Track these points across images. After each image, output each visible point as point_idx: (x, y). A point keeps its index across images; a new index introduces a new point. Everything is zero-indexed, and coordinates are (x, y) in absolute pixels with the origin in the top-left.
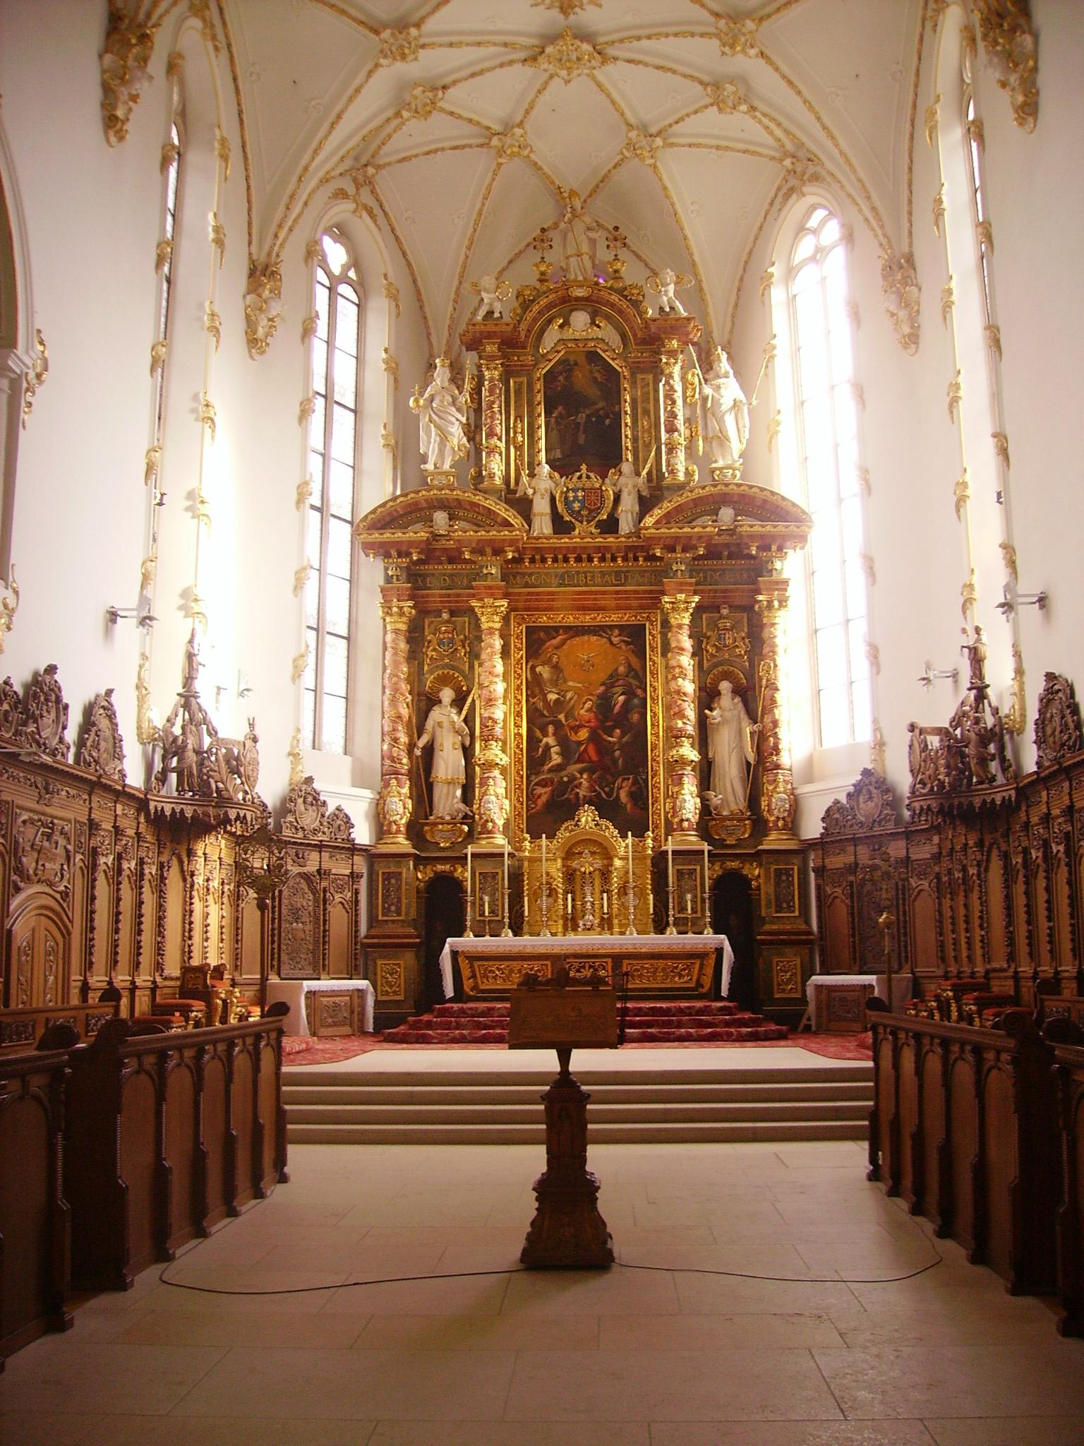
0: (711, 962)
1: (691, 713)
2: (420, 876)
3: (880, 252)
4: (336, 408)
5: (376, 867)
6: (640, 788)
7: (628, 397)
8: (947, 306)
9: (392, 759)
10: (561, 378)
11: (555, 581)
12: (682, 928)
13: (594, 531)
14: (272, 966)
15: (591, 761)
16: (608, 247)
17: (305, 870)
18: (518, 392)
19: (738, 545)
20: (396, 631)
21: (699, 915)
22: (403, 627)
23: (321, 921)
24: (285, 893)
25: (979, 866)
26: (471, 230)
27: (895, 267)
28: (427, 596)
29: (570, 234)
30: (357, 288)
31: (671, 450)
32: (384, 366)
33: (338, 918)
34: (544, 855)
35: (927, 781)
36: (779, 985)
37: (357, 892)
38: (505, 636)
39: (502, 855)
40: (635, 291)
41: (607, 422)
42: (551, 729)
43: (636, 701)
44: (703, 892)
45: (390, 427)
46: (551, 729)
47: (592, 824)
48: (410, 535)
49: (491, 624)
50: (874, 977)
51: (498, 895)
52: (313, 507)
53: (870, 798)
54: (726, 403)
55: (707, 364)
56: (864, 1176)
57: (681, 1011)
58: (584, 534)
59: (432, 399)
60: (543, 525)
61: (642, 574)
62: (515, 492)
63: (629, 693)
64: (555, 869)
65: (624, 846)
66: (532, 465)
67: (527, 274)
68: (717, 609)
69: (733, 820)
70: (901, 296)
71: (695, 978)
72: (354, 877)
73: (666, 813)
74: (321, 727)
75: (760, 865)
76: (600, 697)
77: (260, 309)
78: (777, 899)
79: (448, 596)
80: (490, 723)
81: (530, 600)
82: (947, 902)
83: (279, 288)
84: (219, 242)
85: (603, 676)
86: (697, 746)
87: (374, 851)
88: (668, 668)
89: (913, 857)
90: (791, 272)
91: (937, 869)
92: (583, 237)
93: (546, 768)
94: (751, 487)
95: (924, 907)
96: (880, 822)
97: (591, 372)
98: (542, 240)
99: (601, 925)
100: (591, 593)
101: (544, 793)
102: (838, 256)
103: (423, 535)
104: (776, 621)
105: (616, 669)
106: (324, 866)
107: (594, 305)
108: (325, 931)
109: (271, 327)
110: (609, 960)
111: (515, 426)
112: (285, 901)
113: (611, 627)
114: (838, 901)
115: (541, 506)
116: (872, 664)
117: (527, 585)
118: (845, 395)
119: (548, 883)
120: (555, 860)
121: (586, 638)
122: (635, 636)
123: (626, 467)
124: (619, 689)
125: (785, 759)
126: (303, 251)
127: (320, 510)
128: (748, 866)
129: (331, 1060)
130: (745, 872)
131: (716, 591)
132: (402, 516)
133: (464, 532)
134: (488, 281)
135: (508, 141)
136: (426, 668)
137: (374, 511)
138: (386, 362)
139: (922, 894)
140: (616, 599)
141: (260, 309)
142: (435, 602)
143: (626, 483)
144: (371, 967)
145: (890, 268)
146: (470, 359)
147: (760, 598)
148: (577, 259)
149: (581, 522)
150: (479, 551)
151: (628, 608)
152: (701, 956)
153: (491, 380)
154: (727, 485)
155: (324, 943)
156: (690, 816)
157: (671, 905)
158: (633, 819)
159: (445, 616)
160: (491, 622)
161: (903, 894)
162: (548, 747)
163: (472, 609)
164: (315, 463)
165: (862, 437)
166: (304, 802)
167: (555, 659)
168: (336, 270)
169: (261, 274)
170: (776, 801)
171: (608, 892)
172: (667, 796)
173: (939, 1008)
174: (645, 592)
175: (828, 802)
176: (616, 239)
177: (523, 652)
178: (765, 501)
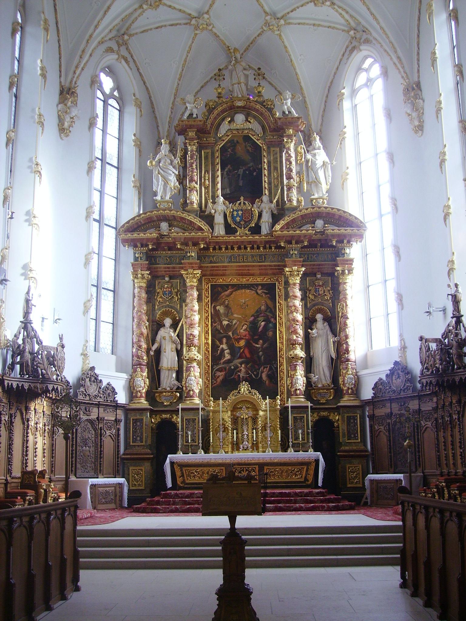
0: (313, 467)
1: (301, 332)
2: (153, 421)
3: (402, 81)
5: (129, 416)
7: (266, 161)
8: (439, 110)
9: (138, 357)
10: (229, 150)
12: (297, 449)
13: (247, 232)
15: (246, 357)
16: (255, 79)
17: (90, 418)
18: (206, 158)
19: (326, 240)
20: (140, 287)
22: (144, 285)
23: (99, 446)
26: (180, 70)
28: (157, 268)
29: (234, 73)
31: (290, 188)
32: (133, 144)
33: (108, 444)
34: (221, 409)
35: (430, 367)
36: (350, 480)
37: (119, 430)
39: (198, 409)
40: (269, 103)
41: (255, 174)
42: (224, 340)
44: (308, 428)
45: (137, 176)
46: (224, 340)
47: (247, 392)
50: (402, 475)
53: (399, 377)
54: (319, 163)
55: (308, 142)
57: (296, 494)
58: (242, 234)
60: (220, 230)
62: (205, 212)
63: (267, 320)
64: (227, 417)
65: (265, 404)
66: (214, 197)
67: (211, 94)
68: (315, 275)
72: (117, 421)
73: (288, 386)
78: (349, 432)
79: (168, 268)
81: (213, 270)
82: (441, 434)
84: (44, 76)
85: (253, 312)
87: (128, 407)
90: (354, 92)
91: (436, 416)
92: (241, 73)
93: (222, 361)
94: (333, 209)
95: (429, 436)
96: (404, 390)
97: (246, 147)
99: (252, 447)
100: (246, 266)
101: (221, 375)
102: (379, 85)
103: (155, 235)
104: (347, 281)
105: (260, 308)
107: (247, 111)
111: (204, 176)
113: (257, 285)
114: (381, 433)
115: (219, 219)
116: (399, 304)
119: (223, 424)
122: (270, 289)
123: (265, 198)
124: (261, 319)
127: (99, 221)
128: (332, 414)
129: (104, 523)
130: (331, 418)
133: (177, 233)
134: (190, 98)
135: (201, 21)
136: (156, 307)
137: (128, 222)
139: (428, 429)
141: (66, 112)
142: (161, 271)
143: (265, 206)
146: (180, 140)
147: (338, 268)
148: (238, 85)
149: (241, 228)
151: (267, 274)
153: (192, 151)
154: (319, 208)
155: (101, 458)
156: (300, 387)
159: (167, 279)
160: (192, 282)
161: (418, 429)
162: (223, 350)
163: (181, 275)
164: (96, 196)
165: (392, 181)
166: (90, 380)
168: (108, 91)
169: (66, 93)
170: (347, 379)
172: (288, 376)
174: (275, 266)
176: (259, 75)
178: (340, 216)
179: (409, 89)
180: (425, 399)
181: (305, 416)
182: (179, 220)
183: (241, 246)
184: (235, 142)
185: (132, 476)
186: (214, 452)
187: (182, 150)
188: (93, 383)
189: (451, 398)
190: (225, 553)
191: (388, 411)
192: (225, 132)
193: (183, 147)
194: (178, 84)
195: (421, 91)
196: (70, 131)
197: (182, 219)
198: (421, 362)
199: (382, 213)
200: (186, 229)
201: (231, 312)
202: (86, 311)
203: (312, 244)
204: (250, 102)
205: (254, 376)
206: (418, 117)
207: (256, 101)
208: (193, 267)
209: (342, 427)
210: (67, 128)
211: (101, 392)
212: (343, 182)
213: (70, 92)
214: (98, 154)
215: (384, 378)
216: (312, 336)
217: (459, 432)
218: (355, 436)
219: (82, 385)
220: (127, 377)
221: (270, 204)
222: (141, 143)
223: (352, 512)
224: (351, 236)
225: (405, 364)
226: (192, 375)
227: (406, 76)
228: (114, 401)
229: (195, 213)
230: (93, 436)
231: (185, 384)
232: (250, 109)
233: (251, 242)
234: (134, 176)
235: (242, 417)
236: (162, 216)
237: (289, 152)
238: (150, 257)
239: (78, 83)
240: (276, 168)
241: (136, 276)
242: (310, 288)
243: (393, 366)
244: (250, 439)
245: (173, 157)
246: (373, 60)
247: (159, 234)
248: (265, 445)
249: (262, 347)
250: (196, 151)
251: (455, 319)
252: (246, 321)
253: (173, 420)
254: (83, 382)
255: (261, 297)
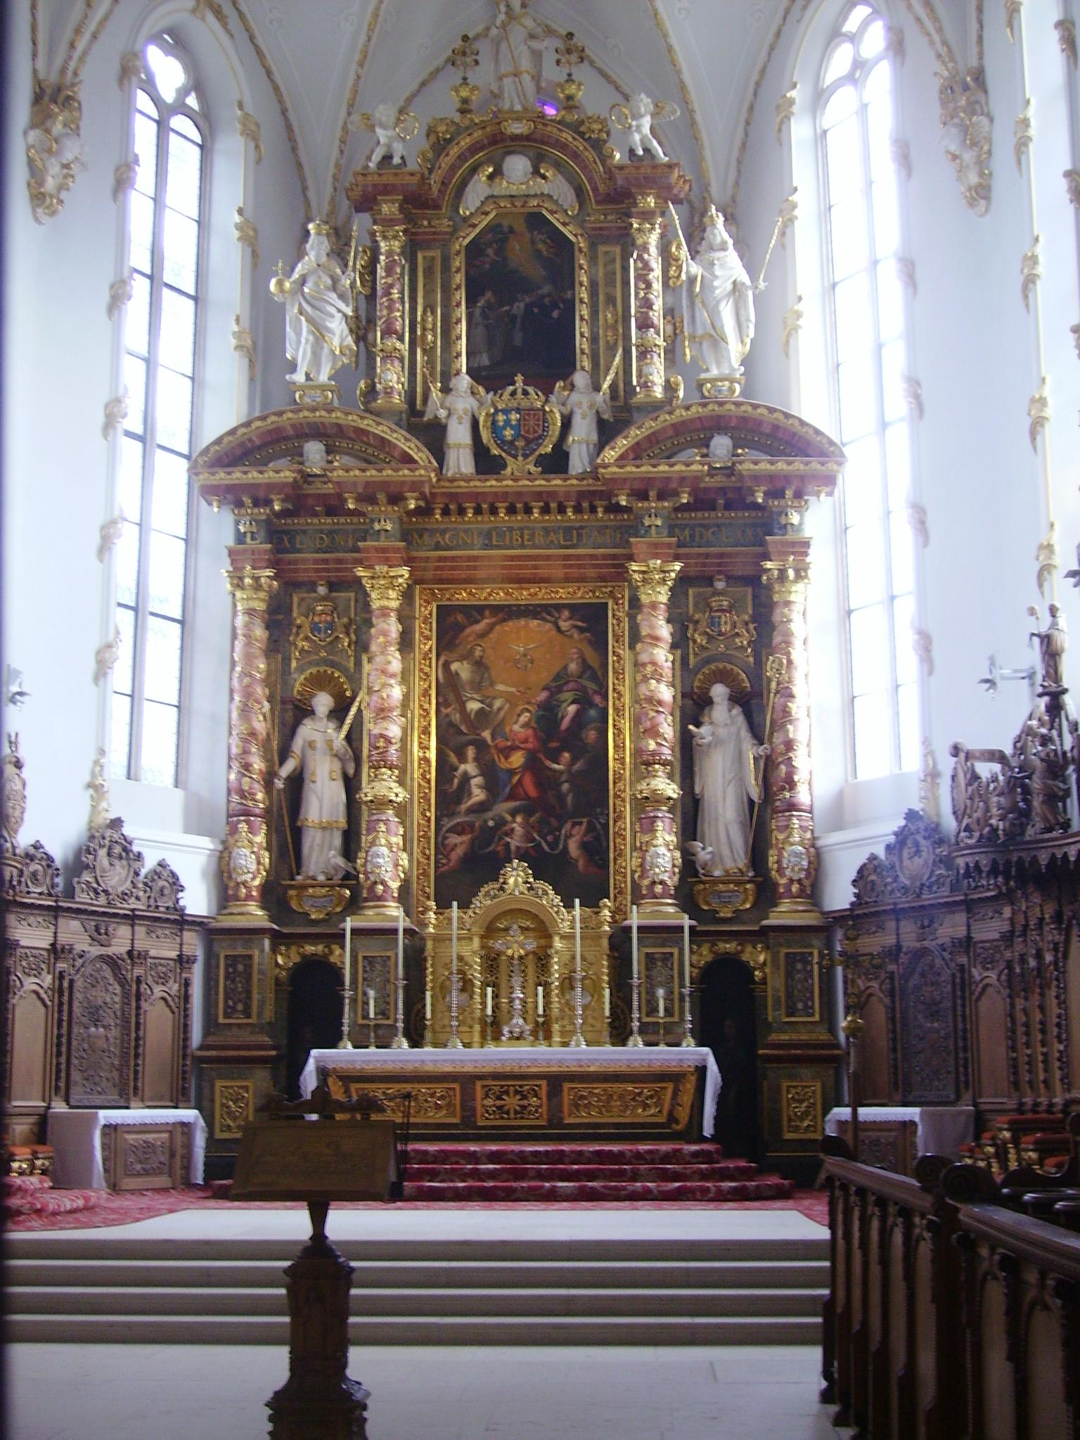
0: (690, 1086)
1: (668, 729)
2: (280, 960)
3: (937, 66)
4: (166, 292)
5: (216, 948)
6: (597, 838)
7: (584, 279)
8: (1022, 144)
9: (242, 794)
10: (490, 251)
11: (478, 541)
12: (652, 1038)
13: (533, 469)
14: (57, 1088)
15: (527, 797)
16: (558, 62)
17: (109, 951)
18: (429, 272)
19: (740, 489)
20: (250, 612)
21: (676, 1019)
22: (261, 606)
23: (132, 1026)
24: (79, 984)
25: (1056, 949)
26: (363, 38)
27: (957, 89)
28: (296, 562)
29: (504, 46)
30: (201, 123)
31: (644, 353)
32: (236, 234)
33: (158, 1020)
34: (455, 932)
35: (974, 826)
36: (790, 1120)
37: (187, 984)
38: (405, 618)
39: (395, 931)
40: (596, 126)
41: (555, 314)
42: (471, 752)
43: (593, 713)
44: (682, 986)
45: (246, 321)
46: (471, 752)
47: (523, 888)
48: (269, 476)
49: (385, 603)
50: (917, 1110)
51: (390, 988)
52: (128, 434)
53: (918, 852)
54: (722, 286)
55: (696, 234)
56: (815, 1397)
57: (639, 1157)
58: (520, 474)
59: (303, 281)
60: (461, 461)
61: (602, 530)
62: (422, 414)
63: (584, 701)
64: (472, 951)
65: (570, 920)
66: (447, 377)
67: (443, 104)
68: (709, 581)
69: (729, 882)
70: (965, 130)
71: (665, 1112)
72: (183, 961)
73: (633, 872)
74: (139, 747)
75: (767, 948)
76: (541, 706)
77: (49, 151)
78: (789, 996)
79: (326, 561)
80: (381, 743)
81: (441, 568)
82: (1020, 1003)
83: (76, 121)
85: (546, 676)
86: (677, 777)
87: (214, 925)
88: (638, 665)
89: (977, 936)
90: (820, 97)
91: (1008, 955)
92: (523, 48)
93: (463, 807)
94: (755, 407)
95: (991, 1009)
96: (930, 887)
97: (533, 242)
98: (464, 54)
99: (534, 1033)
100: (529, 558)
101: (461, 843)
102: (882, 77)
103: (288, 475)
104: (792, 598)
105: (565, 668)
106: (139, 946)
107: (538, 146)
108: (137, 1039)
109: (65, 177)
110: (544, 1083)
111: (423, 320)
112: (78, 996)
113: (559, 607)
114: (873, 999)
115: (459, 434)
116: (922, 661)
117: (438, 547)
118: (890, 276)
119: (460, 972)
120: (471, 939)
121: (523, 622)
122: (592, 620)
123: (580, 379)
124: (567, 696)
125: (803, 796)
126: (116, 67)
127: (141, 439)
128: (749, 948)
129: (120, 1222)
130: (745, 957)
131: (707, 556)
132: (259, 448)
133: (347, 471)
134: (384, 112)
136: (294, 664)
137: (218, 441)
138: (238, 227)
139: (990, 990)
140: (565, 566)
141: (49, 151)
142: (306, 570)
143: (581, 401)
144: (206, 1091)
145: (949, 90)
146: (360, 224)
147: (769, 565)
148: (515, 81)
149: (515, 457)
150: (368, 497)
151: (582, 579)
152: (673, 1077)
153: (390, 254)
154: (721, 404)
155: (137, 1056)
156: (665, 877)
157: (635, 1004)
158: (584, 878)
159: (322, 590)
160: (385, 599)
161: (963, 991)
162: (466, 778)
163: (358, 580)
164: (133, 373)
165: (911, 337)
166: (109, 855)
167: (478, 653)
168: (169, 96)
170: (790, 854)
171: (546, 985)
172: (634, 848)
173: (997, 1155)
174: (605, 557)
175: (860, 858)
176: (569, 51)
177: (433, 643)
178: (776, 428)
179: (956, 88)
180: (982, 912)
181: (676, 951)
182: (352, 435)
183: (517, 504)
184: (506, 229)
185: (223, 1105)
186: (435, 1045)
187: (365, 252)
188: (116, 862)
189: (1037, 906)
190: (295, 1305)
191: (890, 940)
192: (478, 204)
193: (369, 243)
194: (359, 77)
195: (986, 92)
196: (61, 202)
197: (361, 432)
198: (955, 813)
199: (887, 420)
200: (373, 459)
201: (490, 677)
202: (102, 669)
203: (703, 501)
204: (546, 125)
205: (546, 847)
206: (976, 163)
207: (559, 122)
208: (387, 559)
209: (775, 984)
210: (54, 192)
211: (141, 885)
212: (789, 335)
213: (60, 100)
214: (139, 258)
215: (881, 852)
216: (700, 742)
217: (1057, 997)
218: (806, 1007)
219: (87, 867)
220: (211, 846)
221: (594, 394)
222: (255, 230)
223: (779, 1204)
224: (802, 478)
225: (935, 819)
226: (383, 841)
227: (947, 55)
228: (175, 909)
229: (396, 418)
230: (117, 999)
231: (364, 865)
232: (543, 143)
233: (540, 493)
234: (238, 320)
235: (510, 952)
236: (309, 424)
237: (646, 256)
238: (277, 532)
239: (84, 74)
240: (611, 300)
241: (238, 583)
242: (697, 617)
243: (903, 823)
244: (531, 1012)
245: (338, 271)
246: (869, 10)
247: (300, 472)
248: (568, 1028)
249: (569, 770)
250: (402, 254)
251: (1046, 699)
252: (529, 703)
253: (332, 959)
254: (91, 857)
255: (566, 639)
